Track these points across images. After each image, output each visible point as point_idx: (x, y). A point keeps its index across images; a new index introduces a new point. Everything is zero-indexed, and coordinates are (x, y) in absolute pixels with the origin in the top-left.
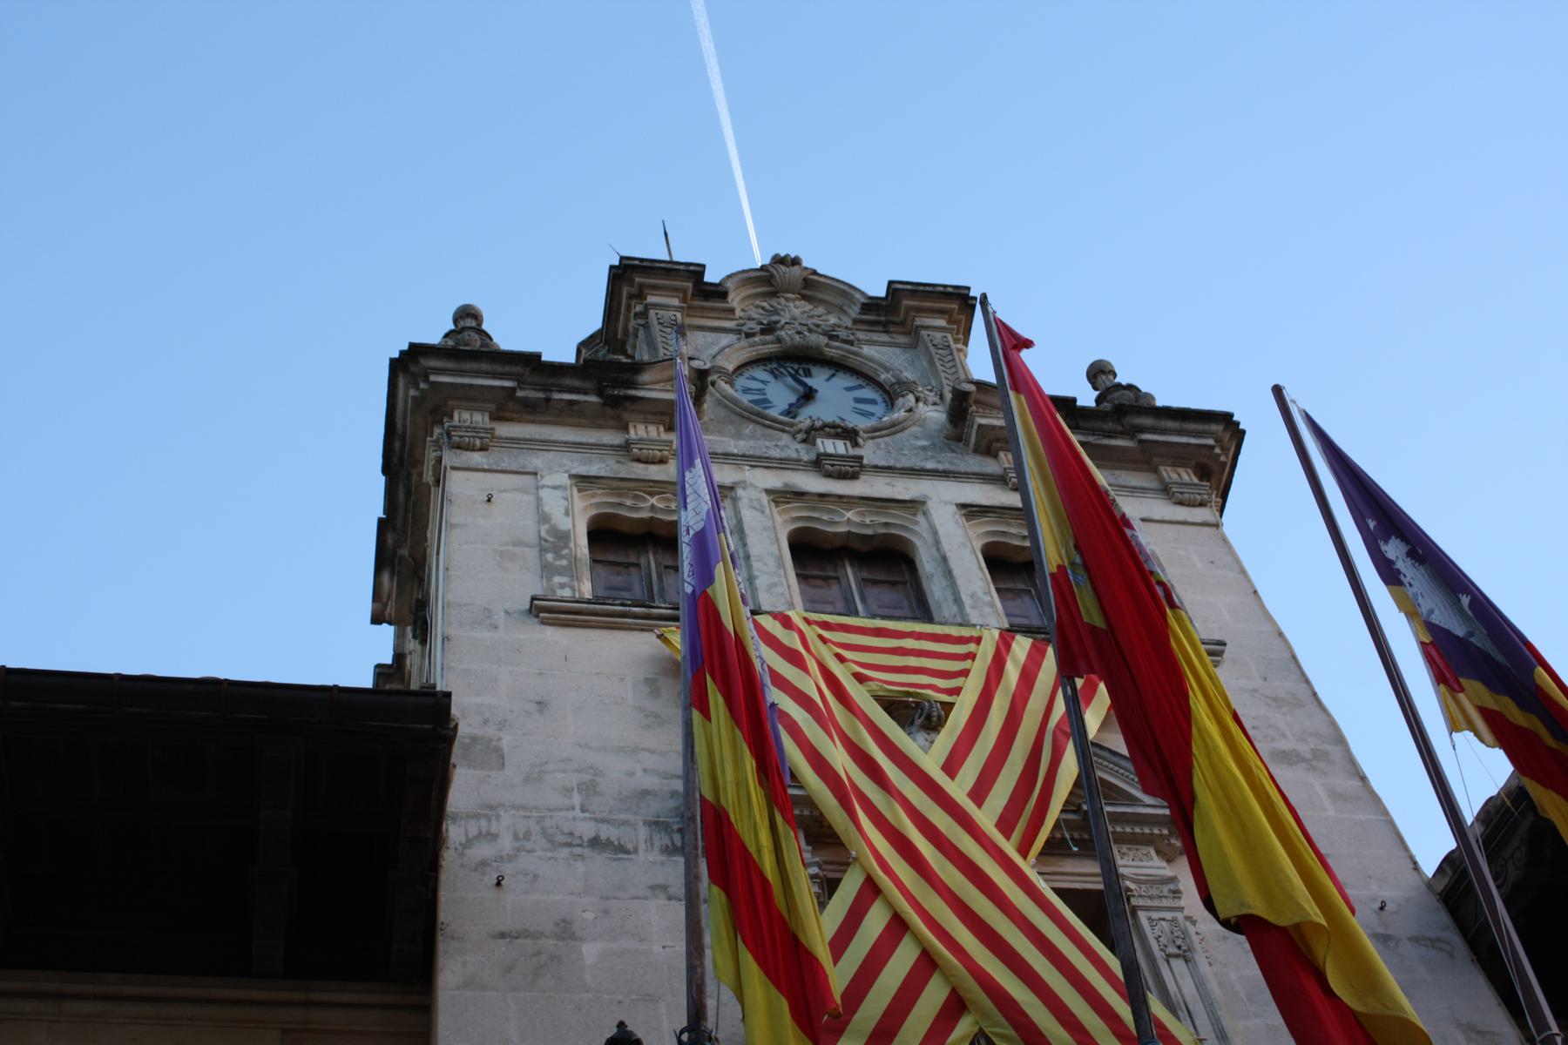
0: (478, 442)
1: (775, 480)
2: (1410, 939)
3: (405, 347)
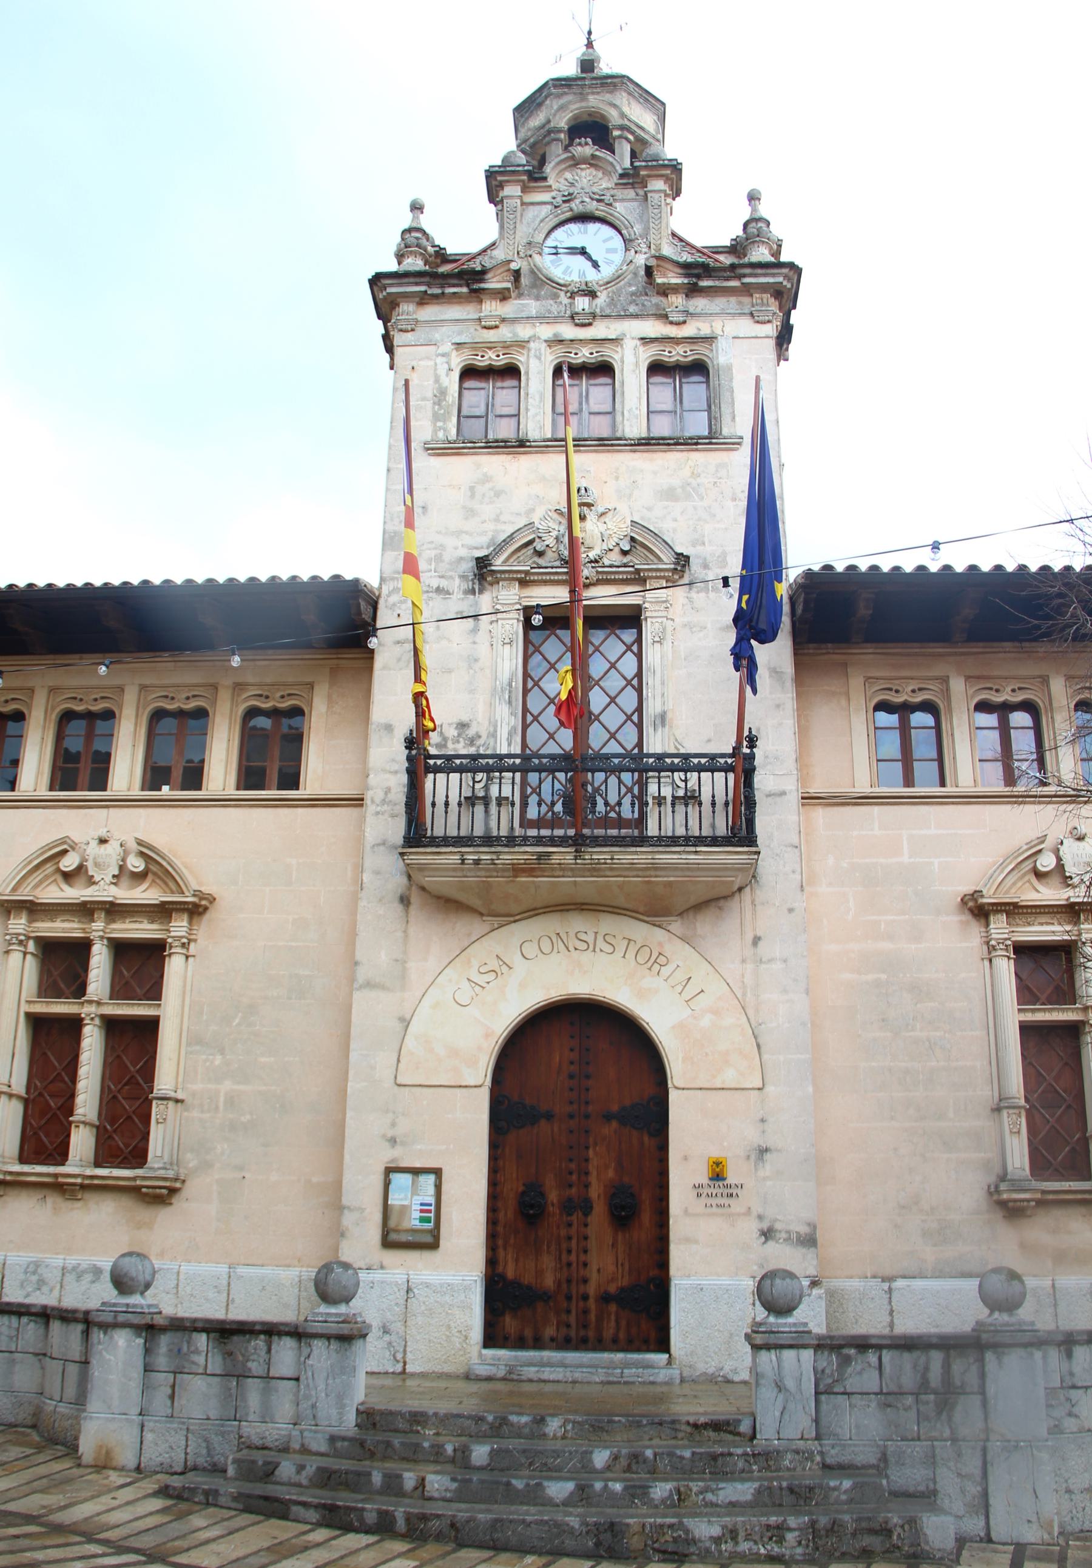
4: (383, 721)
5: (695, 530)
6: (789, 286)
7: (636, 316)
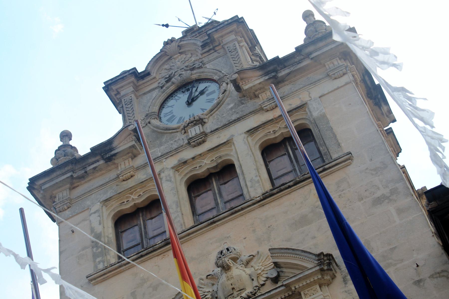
0: (66, 207)
1: (173, 161)
2: (429, 277)
7: (238, 120)
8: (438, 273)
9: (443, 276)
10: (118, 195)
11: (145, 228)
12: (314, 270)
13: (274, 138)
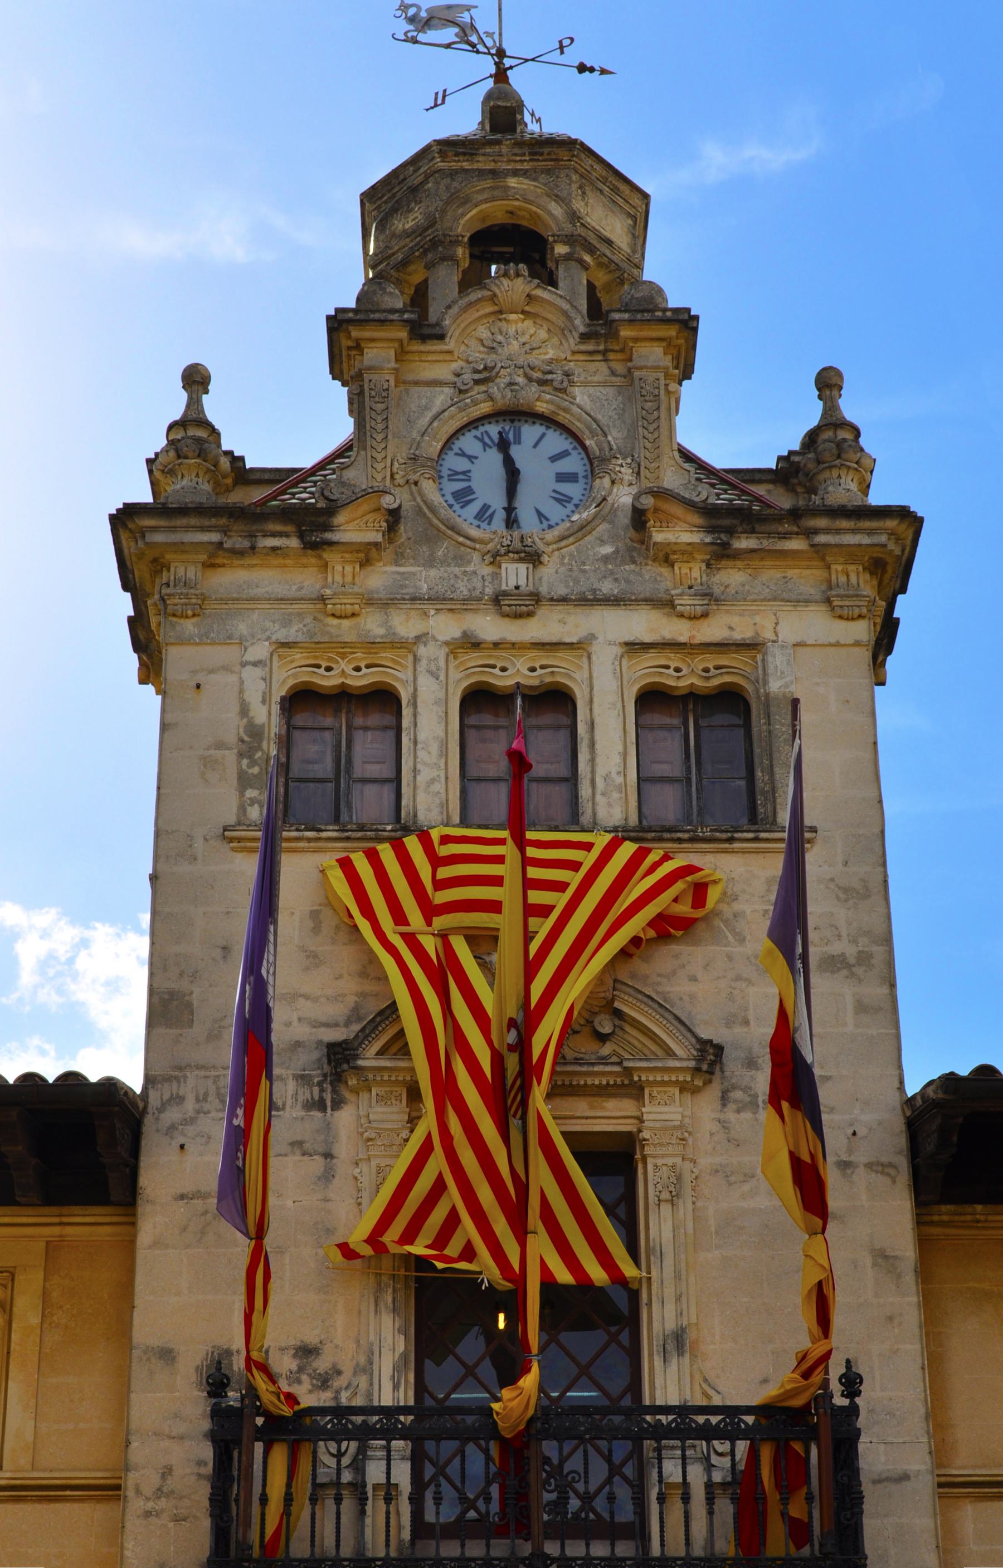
0: (190, 613)
3: (121, 506)
4: (155, 1342)
5: (731, 997)
6: (898, 551)
7: (615, 601)
8: (882, 1165)
9: (888, 1175)
10: (313, 646)
11: (349, 746)
12: (685, 1064)
13: (671, 687)
